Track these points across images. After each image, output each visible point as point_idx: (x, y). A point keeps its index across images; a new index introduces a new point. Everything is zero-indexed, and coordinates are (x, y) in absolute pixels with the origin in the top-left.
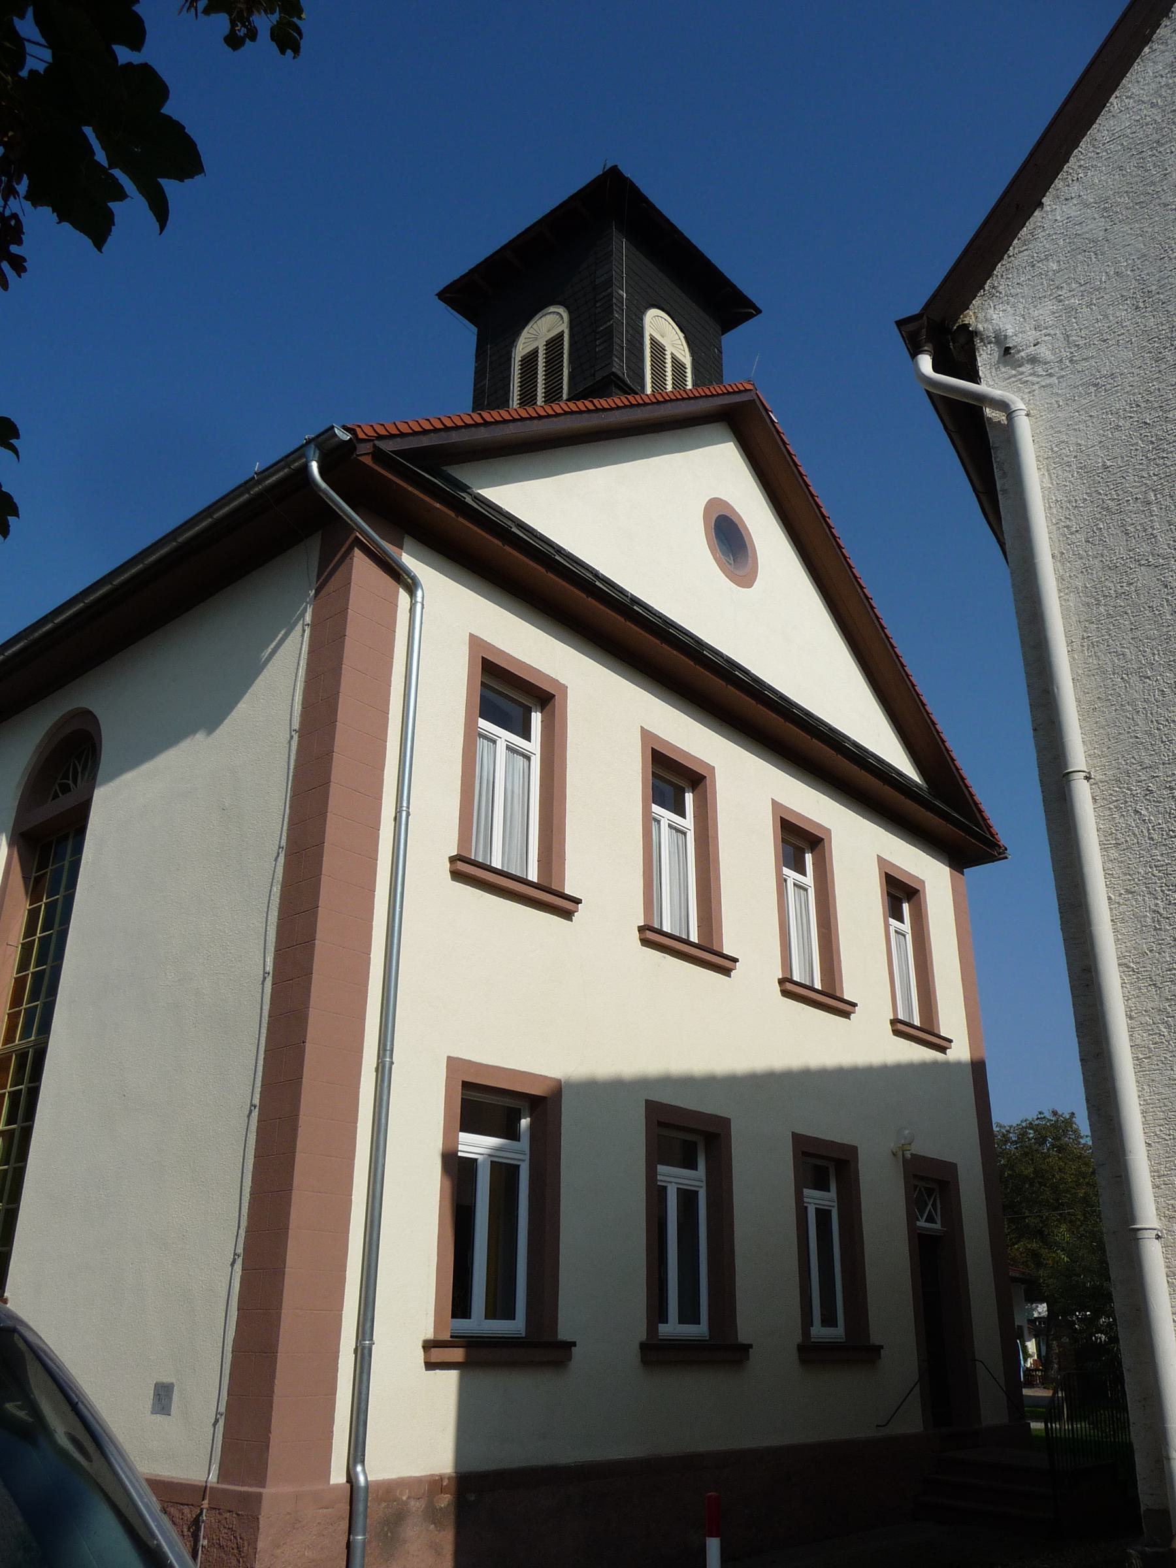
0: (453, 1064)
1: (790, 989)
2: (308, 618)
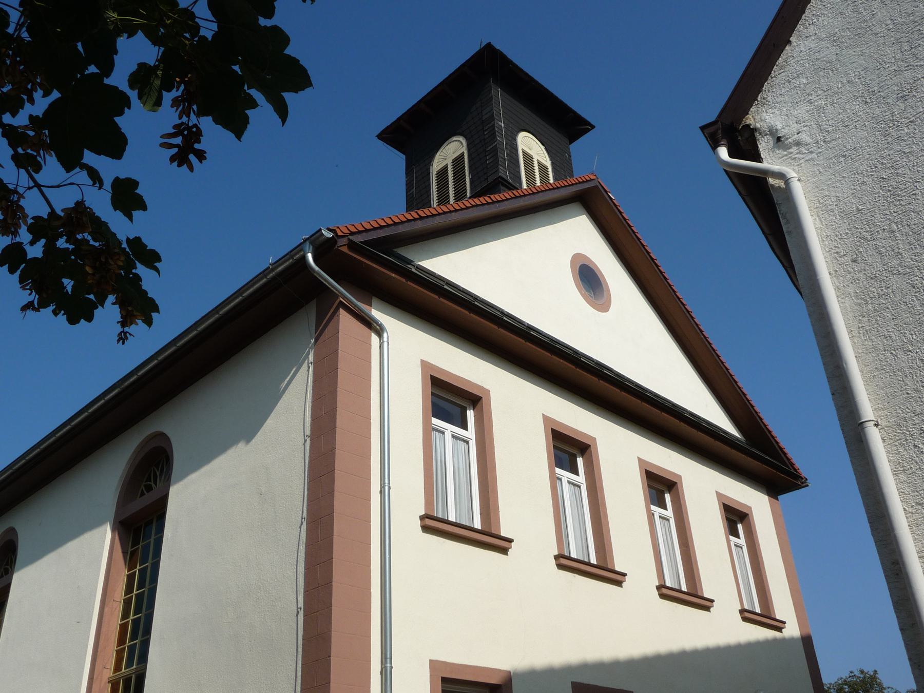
1: (666, 593)
2: (311, 358)
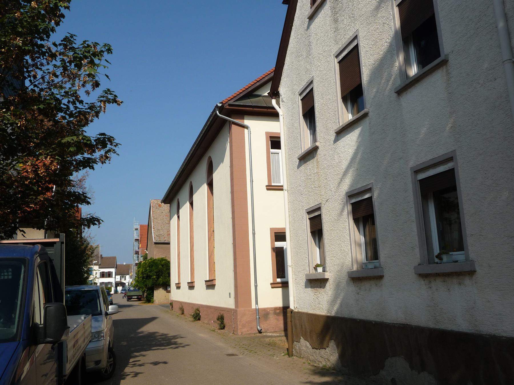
0: (267, 133)
